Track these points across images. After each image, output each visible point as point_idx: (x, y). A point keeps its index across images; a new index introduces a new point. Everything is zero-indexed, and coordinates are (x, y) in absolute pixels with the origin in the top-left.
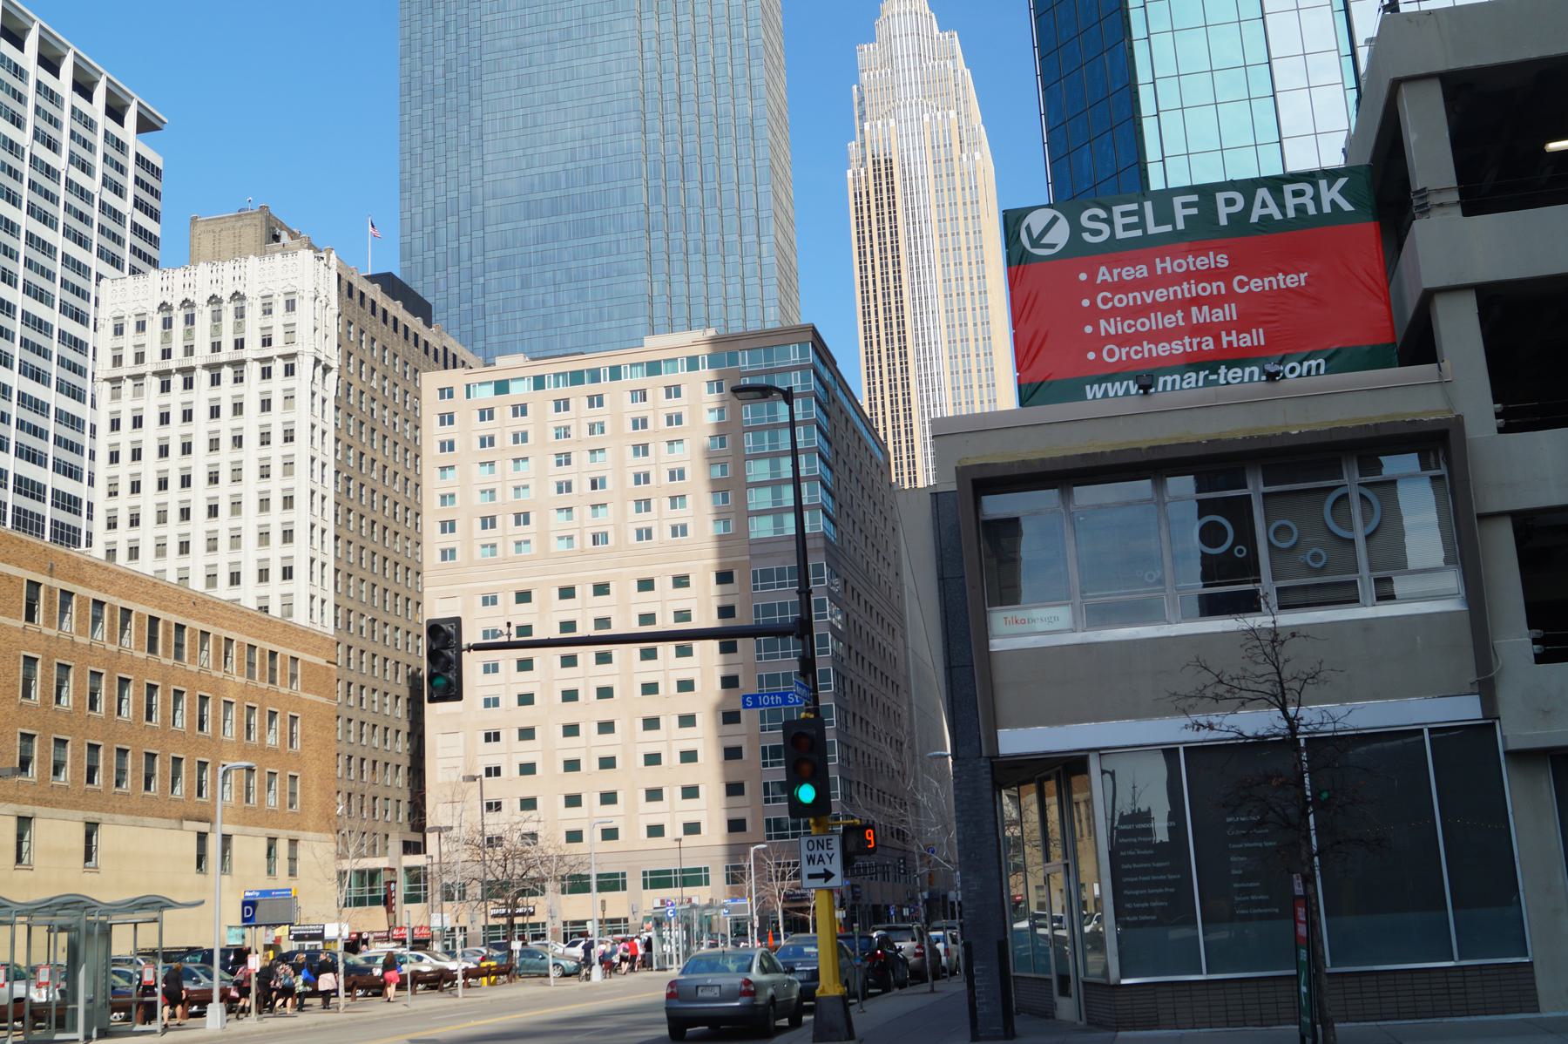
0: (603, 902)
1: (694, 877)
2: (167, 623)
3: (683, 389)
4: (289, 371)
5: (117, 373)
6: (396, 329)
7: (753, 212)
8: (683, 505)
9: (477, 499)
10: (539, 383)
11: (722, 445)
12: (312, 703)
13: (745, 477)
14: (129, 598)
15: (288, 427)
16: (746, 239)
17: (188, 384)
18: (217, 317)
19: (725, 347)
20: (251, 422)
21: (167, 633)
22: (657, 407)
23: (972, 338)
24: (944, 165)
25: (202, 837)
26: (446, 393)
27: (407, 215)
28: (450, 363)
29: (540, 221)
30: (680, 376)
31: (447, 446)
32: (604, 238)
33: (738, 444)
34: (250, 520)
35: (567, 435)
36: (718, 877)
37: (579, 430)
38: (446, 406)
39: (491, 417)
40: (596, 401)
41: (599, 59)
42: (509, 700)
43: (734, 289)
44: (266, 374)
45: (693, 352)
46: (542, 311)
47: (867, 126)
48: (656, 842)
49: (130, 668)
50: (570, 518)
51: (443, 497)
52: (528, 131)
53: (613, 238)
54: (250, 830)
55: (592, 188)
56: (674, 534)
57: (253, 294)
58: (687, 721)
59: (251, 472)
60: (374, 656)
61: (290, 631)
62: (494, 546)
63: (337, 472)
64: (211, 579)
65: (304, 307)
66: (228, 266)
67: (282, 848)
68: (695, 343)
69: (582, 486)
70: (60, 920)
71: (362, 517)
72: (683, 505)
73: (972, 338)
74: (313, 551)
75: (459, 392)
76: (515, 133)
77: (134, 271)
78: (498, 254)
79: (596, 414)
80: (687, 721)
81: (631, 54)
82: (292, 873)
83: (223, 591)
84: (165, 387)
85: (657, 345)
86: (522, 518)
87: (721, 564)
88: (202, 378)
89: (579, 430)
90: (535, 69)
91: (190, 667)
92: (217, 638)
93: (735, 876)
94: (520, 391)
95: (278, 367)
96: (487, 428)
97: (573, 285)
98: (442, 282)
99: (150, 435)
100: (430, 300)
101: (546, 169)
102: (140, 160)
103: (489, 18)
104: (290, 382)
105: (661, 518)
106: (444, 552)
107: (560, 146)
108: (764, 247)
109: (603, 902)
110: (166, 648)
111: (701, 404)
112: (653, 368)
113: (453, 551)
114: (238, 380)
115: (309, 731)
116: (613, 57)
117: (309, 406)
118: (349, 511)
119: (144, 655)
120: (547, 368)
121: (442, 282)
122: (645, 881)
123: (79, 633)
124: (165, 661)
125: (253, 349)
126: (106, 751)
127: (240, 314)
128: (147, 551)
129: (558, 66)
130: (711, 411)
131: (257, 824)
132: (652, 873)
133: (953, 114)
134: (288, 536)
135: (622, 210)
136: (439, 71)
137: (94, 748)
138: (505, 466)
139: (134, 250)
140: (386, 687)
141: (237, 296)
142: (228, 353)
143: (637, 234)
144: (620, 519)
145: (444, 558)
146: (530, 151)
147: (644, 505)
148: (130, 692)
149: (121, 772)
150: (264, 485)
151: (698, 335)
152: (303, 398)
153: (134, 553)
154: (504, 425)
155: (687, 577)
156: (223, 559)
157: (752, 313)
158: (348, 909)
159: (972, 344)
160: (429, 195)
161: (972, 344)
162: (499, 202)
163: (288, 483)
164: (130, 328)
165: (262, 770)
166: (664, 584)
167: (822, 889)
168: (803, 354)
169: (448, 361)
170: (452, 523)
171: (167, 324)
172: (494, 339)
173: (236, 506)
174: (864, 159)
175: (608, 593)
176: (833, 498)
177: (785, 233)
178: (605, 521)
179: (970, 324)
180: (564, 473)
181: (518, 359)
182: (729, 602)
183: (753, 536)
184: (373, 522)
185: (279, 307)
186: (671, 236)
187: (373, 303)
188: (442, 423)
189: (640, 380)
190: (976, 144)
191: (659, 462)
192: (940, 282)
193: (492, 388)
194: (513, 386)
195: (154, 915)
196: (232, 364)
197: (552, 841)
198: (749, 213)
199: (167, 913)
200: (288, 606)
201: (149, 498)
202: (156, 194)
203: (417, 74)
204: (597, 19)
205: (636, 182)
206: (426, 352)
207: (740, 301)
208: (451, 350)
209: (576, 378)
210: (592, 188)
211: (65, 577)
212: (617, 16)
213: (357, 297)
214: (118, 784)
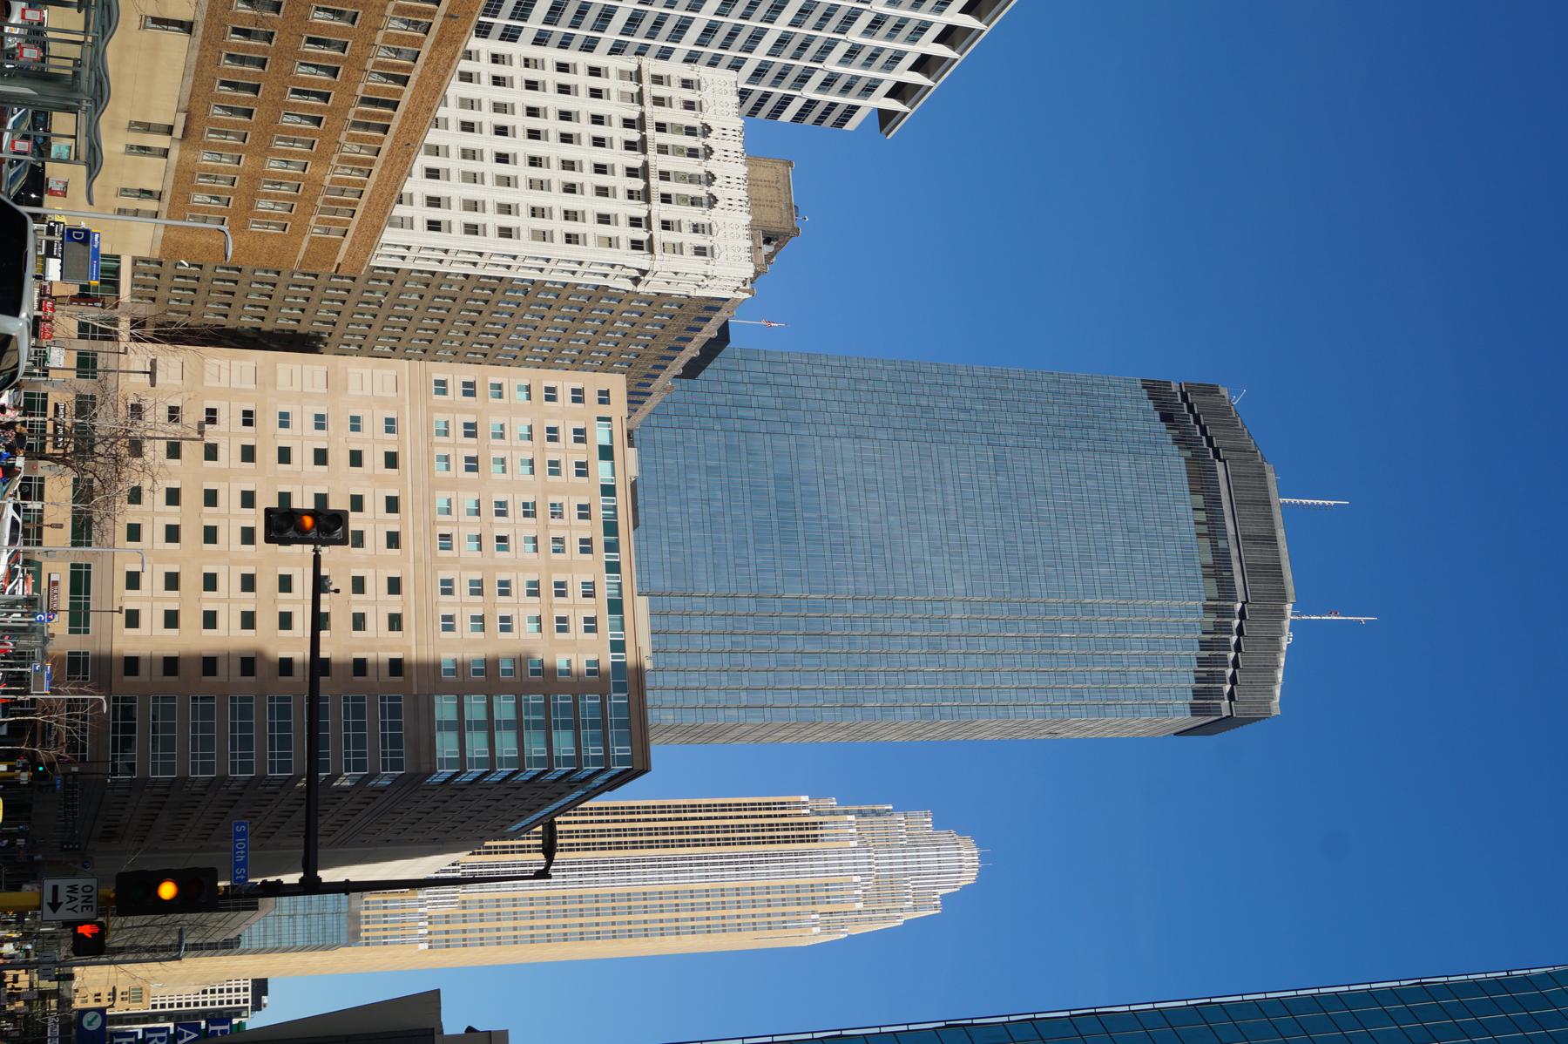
0: (61, 526)
1: (79, 619)
2: (390, 117)
3: (592, 636)
4: (636, 245)
6: (671, 348)
7: (770, 703)
8: (474, 629)
10: (608, 490)
11: (534, 672)
12: (298, 246)
13: (499, 694)
14: (419, 84)
15: (581, 239)
16: (743, 694)
17: (630, 146)
18: (692, 179)
19: (630, 680)
20: (588, 203)
21: (380, 116)
22: (577, 608)
23: (631, 918)
24: (809, 896)
25: (169, 130)
26: (604, 396)
27: (786, 359)
28: (635, 398)
30: (606, 633)
31: (551, 395)
32: (751, 551)
33: (532, 688)
34: (490, 194)
35: (553, 515)
36: (77, 643)
37: (558, 527)
38: (591, 396)
39: (577, 440)
40: (586, 546)
41: (927, 558)
42: (284, 438)
43: (694, 680)
44: (635, 222)
45: (630, 648)
46: (683, 486)
47: (851, 818)
48: (121, 580)
49: (347, 78)
50: (469, 512)
51: (500, 386)
52: (861, 484)
53: (752, 561)
54: (171, 175)
55: (802, 544)
56: (445, 618)
57: (714, 216)
58: (248, 620)
59: (539, 199)
60: (344, 302)
61: (379, 218)
62: (446, 433)
63: (533, 282)
64: (435, 151)
65: (698, 265)
66: (743, 195)
67: (150, 205)
68: (638, 650)
69: (501, 527)
70: (85, 72)
71: (486, 302)
72: (474, 629)
73: (631, 918)
74: (454, 253)
75: (604, 411)
76: (860, 470)
77: (744, 94)
78: (743, 445)
79: (573, 546)
80: (248, 620)
81: (931, 590)
82: (121, 211)
83: (423, 161)
84: (628, 123)
85: (639, 610)
86: (472, 464)
87: (410, 665)
88: (635, 160)
89: (558, 527)
90: (920, 495)
91: (344, 135)
92: (371, 162)
93: (76, 664)
94: (602, 471)
95: (641, 234)
96: (566, 435)
97: (707, 518)
98: (719, 388)
99: (582, 104)
100: (701, 376)
101: (823, 499)
102: (853, 109)
103: (972, 453)
104: (625, 244)
105: (463, 606)
106: (443, 383)
108: (734, 712)
109: (61, 526)
110: (363, 114)
111: (575, 653)
112: (615, 606)
113: (444, 392)
114: (631, 194)
115: (269, 240)
116: (929, 572)
117: (601, 261)
118: (493, 291)
119: (360, 92)
120: (622, 499)
121: (719, 388)
122: (80, 566)
123: (387, 36)
124: (352, 113)
125: (660, 211)
126: (265, 48)
127: (695, 202)
128: (468, 91)
129: (923, 517)
130: (569, 662)
131: (176, 182)
132: (88, 574)
133: (859, 906)
134: (472, 229)
135: (779, 571)
136: (923, 401)
137: (269, 37)
138: (527, 451)
139: (766, 96)
140: (310, 311)
141: (713, 201)
143: (754, 585)
144: (465, 562)
145: (438, 383)
146: (841, 484)
147: (477, 589)
148: (324, 77)
149: (242, 60)
150: (525, 211)
151: (647, 651)
152: (609, 255)
153: (467, 77)
154: (568, 452)
155: (400, 629)
156: (453, 164)
157: (669, 697)
160: (804, 382)
161: (626, 918)
162: (794, 450)
163: (524, 234)
164: (688, 95)
165: (233, 192)
166: (394, 604)
167: (41, 899)
168: (621, 760)
169: (636, 397)
170: (473, 394)
171: (691, 131)
172: (658, 436)
173: (506, 181)
174: (819, 814)
175: (389, 546)
176: (471, 783)
177: (748, 733)
178: (464, 548)
179: (646, 917)
180: (515, 510)
181: (633, 471)
182: (370, 671)
183: (437, 699)
184: (480, 312)
185: (699, 240)
186: (751, 619)
187: (699, 330)
188: (574, 391)
189: (603, 593)
190: (828, 928)
191: (521, 607)
192: (691, 887)
193: (607, 443)
194: (607, 464)
195: (83, 156)
196: (647, 189)
197: (127, 557)
198: (769, 698)
199: (83, 169)
200: (401, 223)
201: (520, 97)
202: (819, 121)
204: (966, 559)
205: (806, 587)
206: (648, 376)
207: (681, 685)
208: (648, 400)
209: (611, 528)
211: (443, 28)
212: (968, 581)
213: (706, 314)
214: (229, 56)
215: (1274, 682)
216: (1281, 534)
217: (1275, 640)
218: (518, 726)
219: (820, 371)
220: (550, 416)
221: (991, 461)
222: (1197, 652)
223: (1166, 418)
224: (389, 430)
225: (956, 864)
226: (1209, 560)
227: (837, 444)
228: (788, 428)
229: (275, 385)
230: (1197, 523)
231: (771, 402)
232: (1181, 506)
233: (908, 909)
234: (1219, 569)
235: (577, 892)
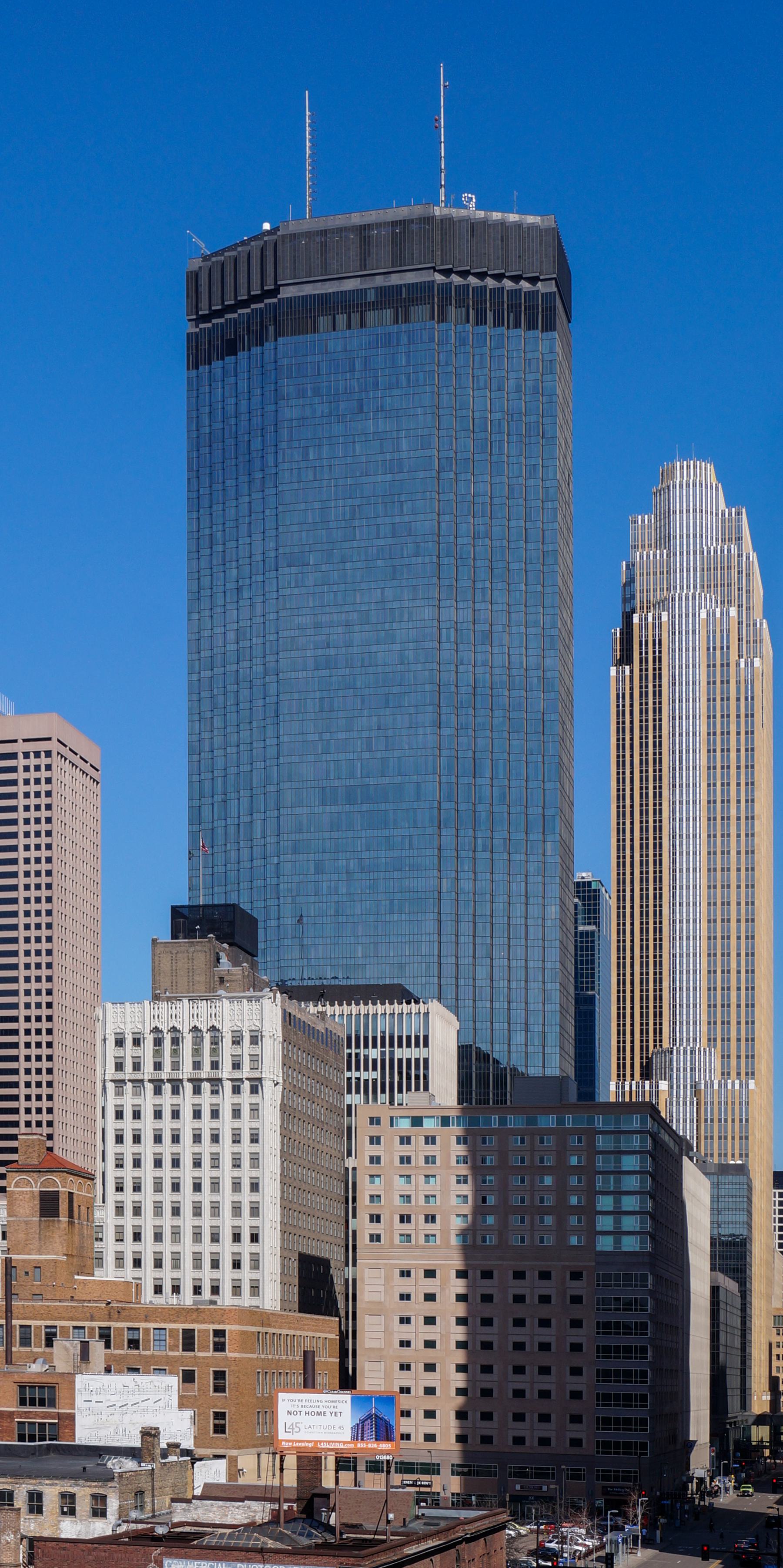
4: (254, 1090)
5: (120, 1076)
9: (397, 1201)
23: (733, 868)
24: (719, 669)
29: (334, 809)
38: (374, 1130)
43: (518, 887)
44: (236, 1090)
46: (335, 898)
51: (372, 1196)
55: (387, 780)
73: (733, 868)
75: (385, 1121)
86: (431, 1218)
95: (247, 1085)
96: (405, 1150)
101: (342, 756)
103: (287, 592)
107: (355, 734)
108: (549, 846)
133: (733, 611)
136: (231, 636)
142: (206, 1071)
146: (327, 736)
154: (418, 1150)
158: (16, 1388)
159: (733, 873)
160: (220, 763)
161: (733, 873)
166: (532, 1275)
168: (643, 1122)
171: (158, 1042)
179: (733, 853)
183: (598, 1249)
194: (425, 1121)
203: (206, 633)
204: (396, 605)
207: (523, 899)
210: (387, 780)
212: (418, 603)
215: (519, 226)
216: (356, 219)
217: (475, 228)
218: (618, 1194)
219: (207, 743)
220: (392, 1162)
221: (294, 570)
222: (488, 329)
223: (231, 348)
224: (408, 1274)
225: (698, 490)
226: (388, 313)
227: (285, 739)
228: (272, 788)
229: (380, 1349)
230: (349, 327)
231: (245, 802)
232: (331, 346)
233: (740, 548)
234: (399, 301)
235: (705, 925)
